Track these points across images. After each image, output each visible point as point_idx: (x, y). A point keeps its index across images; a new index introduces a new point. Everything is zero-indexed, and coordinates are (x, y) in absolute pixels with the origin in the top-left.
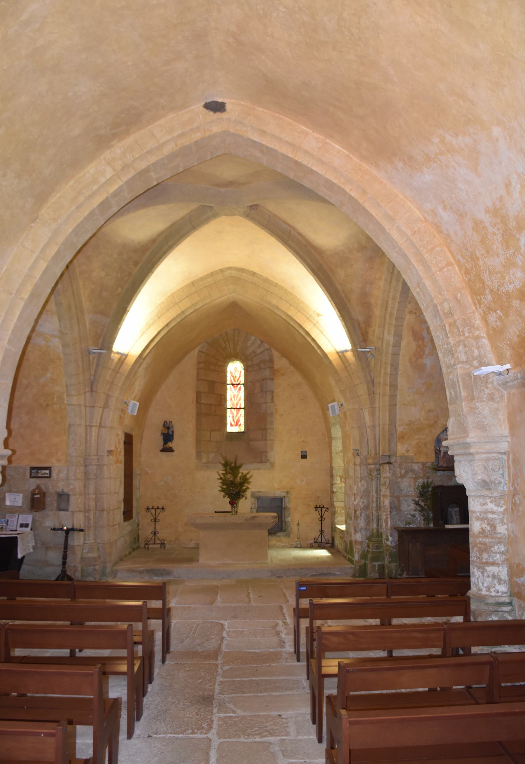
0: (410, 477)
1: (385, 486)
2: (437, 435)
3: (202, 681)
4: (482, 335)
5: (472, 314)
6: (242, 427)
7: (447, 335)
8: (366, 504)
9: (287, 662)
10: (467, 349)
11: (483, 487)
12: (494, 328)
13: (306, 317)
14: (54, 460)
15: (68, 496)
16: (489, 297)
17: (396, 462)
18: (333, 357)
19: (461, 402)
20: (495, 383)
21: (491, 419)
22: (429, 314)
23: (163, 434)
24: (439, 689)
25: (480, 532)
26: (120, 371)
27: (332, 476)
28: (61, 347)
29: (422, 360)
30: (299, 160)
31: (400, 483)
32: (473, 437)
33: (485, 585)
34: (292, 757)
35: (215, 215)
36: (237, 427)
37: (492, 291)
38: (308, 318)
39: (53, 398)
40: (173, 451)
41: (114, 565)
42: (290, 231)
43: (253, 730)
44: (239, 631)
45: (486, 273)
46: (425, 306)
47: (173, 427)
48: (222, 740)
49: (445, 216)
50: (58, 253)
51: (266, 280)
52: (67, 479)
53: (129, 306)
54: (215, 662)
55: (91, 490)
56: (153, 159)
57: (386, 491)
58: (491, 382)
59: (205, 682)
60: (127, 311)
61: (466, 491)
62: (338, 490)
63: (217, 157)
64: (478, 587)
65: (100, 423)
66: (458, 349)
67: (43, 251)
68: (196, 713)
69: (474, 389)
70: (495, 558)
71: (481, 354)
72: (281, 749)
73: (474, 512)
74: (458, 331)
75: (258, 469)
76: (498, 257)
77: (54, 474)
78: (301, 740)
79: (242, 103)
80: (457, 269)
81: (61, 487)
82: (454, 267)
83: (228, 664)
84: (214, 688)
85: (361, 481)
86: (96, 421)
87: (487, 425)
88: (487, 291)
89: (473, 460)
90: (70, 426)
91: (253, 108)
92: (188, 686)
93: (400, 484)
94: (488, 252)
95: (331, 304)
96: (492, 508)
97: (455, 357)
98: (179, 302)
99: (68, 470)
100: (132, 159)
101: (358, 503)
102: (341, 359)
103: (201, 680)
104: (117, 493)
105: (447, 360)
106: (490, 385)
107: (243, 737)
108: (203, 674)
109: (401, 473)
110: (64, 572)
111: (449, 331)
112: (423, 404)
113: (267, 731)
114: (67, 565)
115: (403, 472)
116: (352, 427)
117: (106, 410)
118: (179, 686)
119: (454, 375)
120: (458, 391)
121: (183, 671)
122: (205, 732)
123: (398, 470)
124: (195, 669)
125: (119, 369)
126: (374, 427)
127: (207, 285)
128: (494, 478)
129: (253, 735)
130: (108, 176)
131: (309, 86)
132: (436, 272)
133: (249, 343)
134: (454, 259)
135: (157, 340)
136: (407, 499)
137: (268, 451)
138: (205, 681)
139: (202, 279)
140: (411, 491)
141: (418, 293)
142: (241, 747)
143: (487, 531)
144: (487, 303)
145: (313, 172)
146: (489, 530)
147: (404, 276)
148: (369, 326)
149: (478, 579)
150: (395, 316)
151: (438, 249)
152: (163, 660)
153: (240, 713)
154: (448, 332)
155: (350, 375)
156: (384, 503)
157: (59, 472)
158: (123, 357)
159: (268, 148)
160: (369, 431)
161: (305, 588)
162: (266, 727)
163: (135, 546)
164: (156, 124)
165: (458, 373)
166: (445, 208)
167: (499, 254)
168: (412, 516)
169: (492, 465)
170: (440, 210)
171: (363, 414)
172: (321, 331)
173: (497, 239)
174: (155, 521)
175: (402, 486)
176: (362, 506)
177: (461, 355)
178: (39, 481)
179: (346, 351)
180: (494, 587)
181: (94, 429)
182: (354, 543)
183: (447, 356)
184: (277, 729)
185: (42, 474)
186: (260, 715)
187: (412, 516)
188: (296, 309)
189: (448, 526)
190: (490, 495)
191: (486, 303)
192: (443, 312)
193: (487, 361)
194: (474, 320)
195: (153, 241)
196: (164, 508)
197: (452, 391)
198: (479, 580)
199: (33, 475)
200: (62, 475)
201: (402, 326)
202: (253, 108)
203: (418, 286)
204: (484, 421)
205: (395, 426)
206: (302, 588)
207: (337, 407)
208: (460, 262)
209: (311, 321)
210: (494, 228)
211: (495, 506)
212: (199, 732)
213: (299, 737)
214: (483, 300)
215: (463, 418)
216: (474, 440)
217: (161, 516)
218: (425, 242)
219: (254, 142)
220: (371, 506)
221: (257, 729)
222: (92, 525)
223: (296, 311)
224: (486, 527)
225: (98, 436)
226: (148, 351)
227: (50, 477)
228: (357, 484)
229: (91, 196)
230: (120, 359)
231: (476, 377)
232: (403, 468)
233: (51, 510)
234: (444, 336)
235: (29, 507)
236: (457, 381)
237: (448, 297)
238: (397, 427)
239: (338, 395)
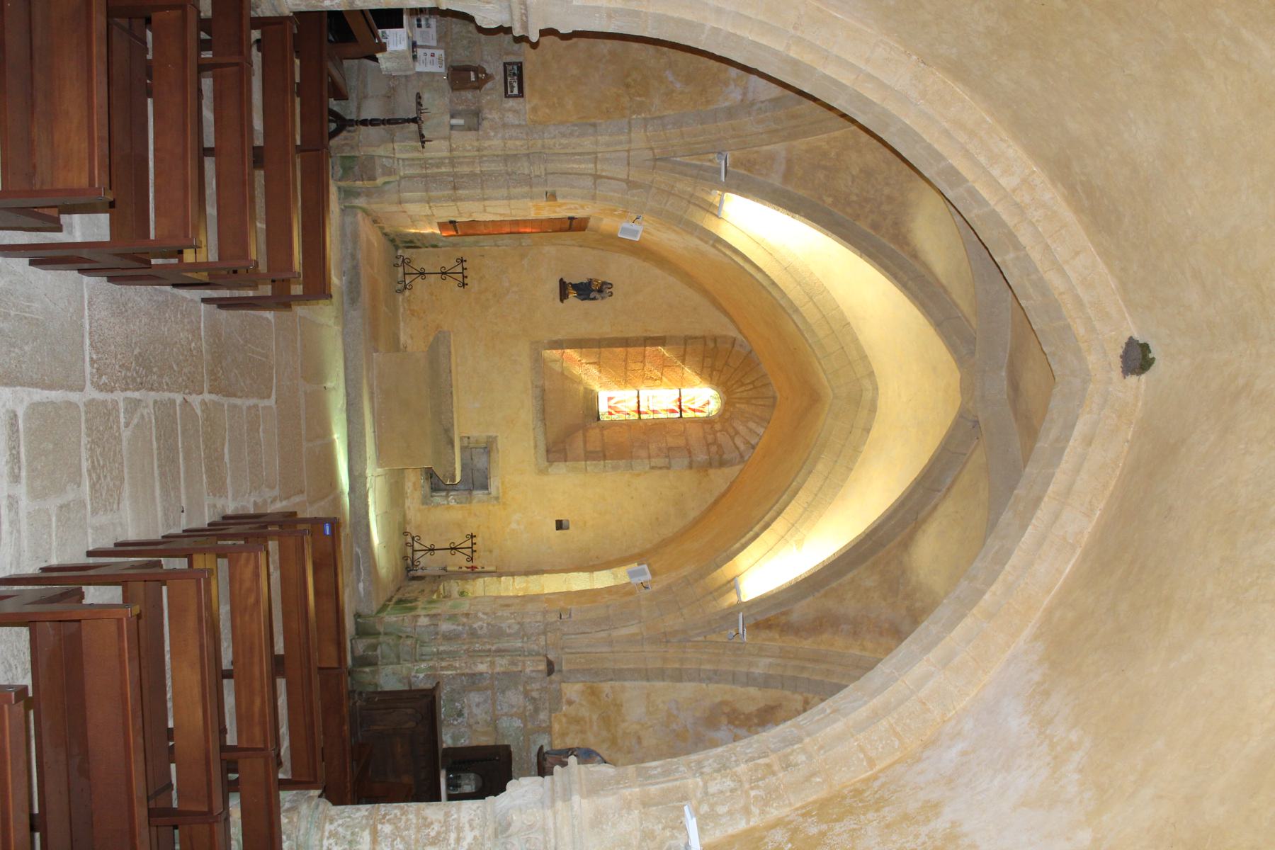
0: (525, 707)
1: (509, 665)
2: (599, 751)
3: (174, 371)
4: (752, 819)
5: (787, 802)
6: (607, 417)
7: (751, 761)
8: (479, 632)
9: (209, 507)
10: (728, 794)
11: (500, 824)
12: (762, 838)
13: (796, 523)
14: (535, 101)
15: (477, 129)
16: (813, 830)
17: (551, 683)
18: (728, 570)
19: (640, 786)
20: (672, 842)
21: (612, 835)
22: (787, 730)
23: (590, 282)
24: (171, 743)
25: (425, 819)
26: (691, 206)
27: (527, 573)
28: (727, 104)
29: (726, 723)
30: (1043, 504)
31: (516, 690)
32: (581, 805)
33: (340, 829)
34: (59, 520)
35: (960, 361)
36: (607, 410)
37: (823, 834)
38: (793, 525)
39: (640, 96)
40: (562, 300)
41: (365, 211)
42: (939, 491)
43: (99, 458)
44: (259, 426)
45: (855, 824)
46: (802, 723)
47: (603, 298)
48: (82, 409)
49: (951, 755)
50: (868, 103)
51: (857, 451)
52: (505, 126)
53: (802, 218)
54: (205, 389)
55: (487, 167)
56: (1036, 255)
57: (501, 665)
58: (674, 834)
59: (173, 376)
60: (795, 215)
61: (493, 797)
62: (502, 585)
63: (1048, 363)
64: (336, 817)
65: (600, 177)
66: (729, 778)
67: (870, 77)
68: (123, 365)
69: (660, 807)
70: (383, 845)
71: (720, 817)
72: (70, 502)
73: (459, 811)
74: (758, 780)
75: (536, 447)
76: (878, 844)
77: (511, 103)
78: (86, 533)
79: (1140, 404)
80: (863, 776)
81: (491, 115)
82: (867, 771)
83: (203, 411)
84: (164, 391)
85: (519, 623)
86: (605, 169)
87: (602, 829)
88: (824, 827)
89: (543, 807)
90: (594, 125)
91: (1132, 423)
92: (166, 349)
93: (514, 691)
94: (888, 826)
95: (818, 565)
96: (465, 838)
97: (715, 774)
98: (814, 303)
99: (519, 126)
100: (1034, 220)
101: (481, 620)
102: (725, 585)
103: (175, 368)
104: (485, 211)
105: (711, 761)
106: (668, 834)
107: (88, 442)
108: (186, 370)
109: (532, 690)
110: (352, 123)
111: (758, 764)
112: (651, 726)
113: (99, 478)
114: (363, 128)
115: (535, 694)
116: (608, 607)
117: (624, 185)
118: (166, 333)
119: (685, 773)
120: (658, 780)
121: (190, 338)
122: (95, 380)
123: (536, 686)
124: (194, 358)
125: (695, 204)
126: (610, 643)
127: (845, 348)
128: (514, 842)
129: (91, 457)
130: (1004, 182)
131: (1166, 517)
132: (856, 740)
133: (752, 425)
134: (881, 771)
135: (747, 267)
136: (489, 701)
137: (567, 463)
138: (175, 376)
139: (855, 340)
140: (502, 709)
141: (823, 710)
142: (73, 439)
143: (427, 831)
144: (805, 827)
145: (1024, 528)
146: (429, 835)
147: (851, 686)
148: (782, 631)
149: (349, 817)
150: (799, 676)
151: (897, 743)
152: (204, 300)
153: (126, 434)
154: (756, 761)
155: (698, 600)
156: (482, 663)
157: (516, 112)
158: (714, 210)
159: (1063, 449)
160: (603, 634)
161: (328, 533)
162: (105, 477)
163: (398, 242)
164: (1098, 258)
165: (688, 780)
166: (964, 753)
167: (884, 845)
168: (461, 711)
169: (536, 838)
170: (960, 746)
171: (633, 625)
172: (773, 548)
173: (908, 842)
174: (443, 273)
175: (510, 693)
176: (475, 626)
177: (718, 785)
178: (499, 77)
179: (738, 594)
180: (336, 844)
181: (592, 166)
182: (413, 613)
183: (718, 761)
184: (101, 495)
185: (511, 83)
186: (123, 466)
187: (461, 711)
188: (809, 504)
189: (443, 774)
190: (487, 836)
191: (804, 825)
192: (791, 754)
193: (709, 827)
194: (776, 806)
195: (915, 256)
196: (466, 286)
197: (659, 770)
198: (349, 820)
199: (509, 68)
200: (511, 118)
201: (783, 687)
202: (1132, 423)
203: (834, 711)
204: (608, 824)
205: (611, 680)
206: (327, 528)
207: (642, 579)
208: (874, 781)
209: (788, 531)
210: (926, 835)
211: (468, 844)
212: (95, 371)
213: (90, 531)
214: (810, 820)
215: (612, 789)
216: (576, 807)
217: (451, 284)
218: (908, 721)
219: (1074, 426)
220: (476, 640)
221: (101, 463)
222: (429, 171)
223: (806, 505)
224: (433, 829)
225: (580, 174)
226: (728, 252)
227: (507, 96)
228: (513, 616)
229: (968, 155)
230: (711, 205)
231: (681, 809)
232: (540, 694)
233: (451, 101)
234: (750, 755)
235: (455, 64)
236: (675, 777)
237: (815, 761)
238: (610, 682)
239: (664, 581)
